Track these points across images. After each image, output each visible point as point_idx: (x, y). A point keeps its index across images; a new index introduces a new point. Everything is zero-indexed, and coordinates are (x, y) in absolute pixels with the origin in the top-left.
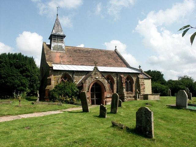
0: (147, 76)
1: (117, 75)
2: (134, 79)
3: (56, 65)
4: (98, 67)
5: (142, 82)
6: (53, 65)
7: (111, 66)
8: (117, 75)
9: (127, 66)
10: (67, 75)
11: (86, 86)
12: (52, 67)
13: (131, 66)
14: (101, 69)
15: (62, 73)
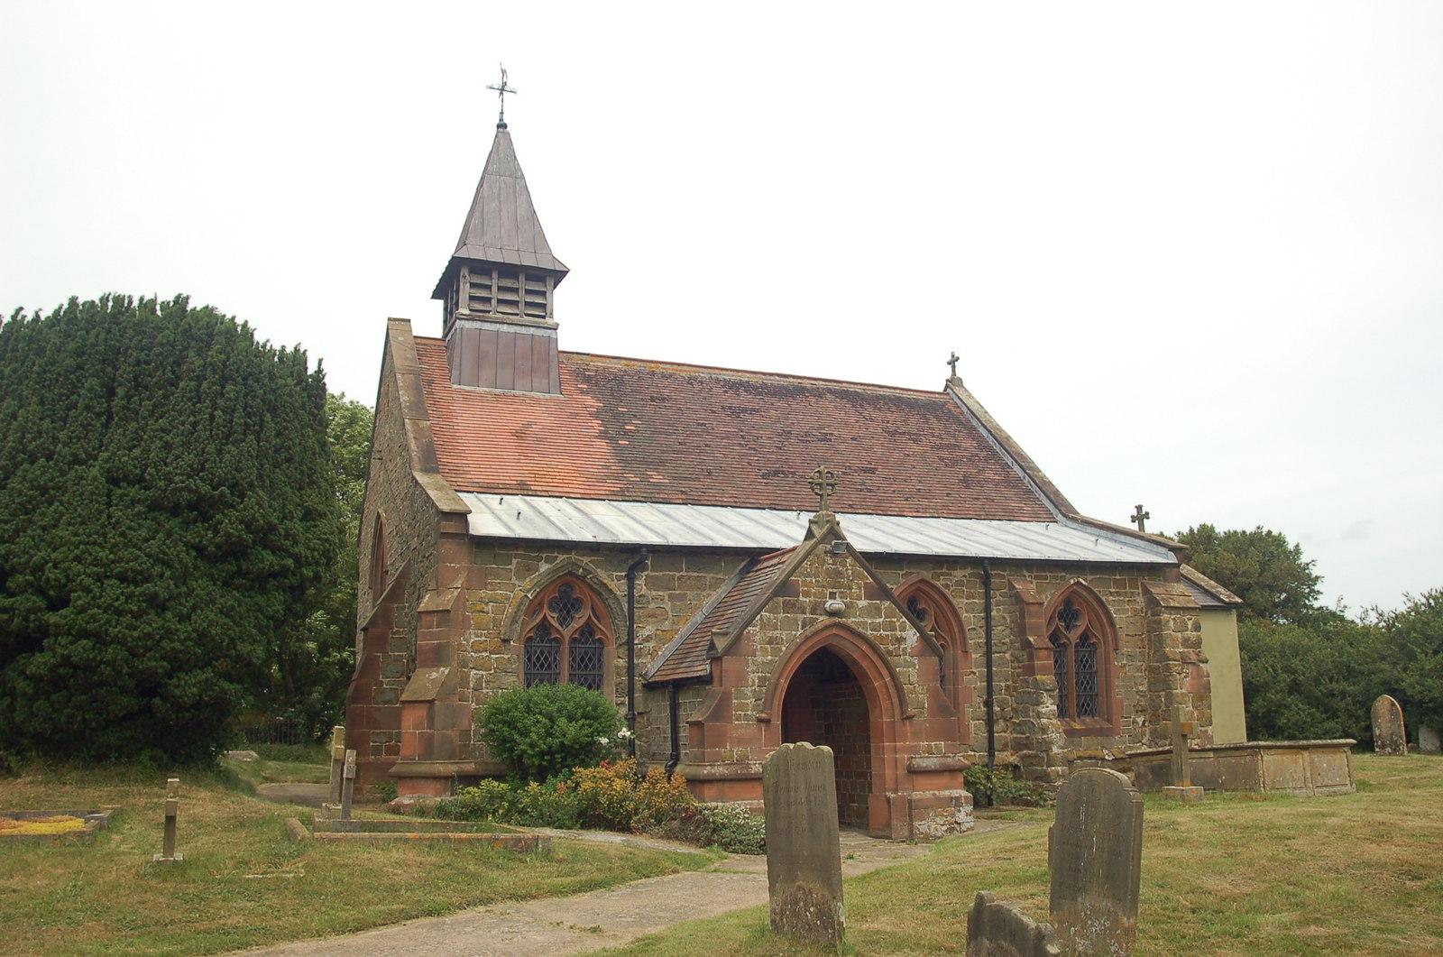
0: (1207, 592)
1: (986, 582)
2: (1124, 611)
3: (493, 500)
4: (839, 517)
5: (1186, 642)
6: (469, 500)
7: (919, 513)
8: (986, 582)
9: (1032, 495)
10: (575, 583)
11: (741, 678)
12: (462, 516)
13: (1085, 510)
14: (867, 532)
15: (544, 567)
